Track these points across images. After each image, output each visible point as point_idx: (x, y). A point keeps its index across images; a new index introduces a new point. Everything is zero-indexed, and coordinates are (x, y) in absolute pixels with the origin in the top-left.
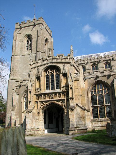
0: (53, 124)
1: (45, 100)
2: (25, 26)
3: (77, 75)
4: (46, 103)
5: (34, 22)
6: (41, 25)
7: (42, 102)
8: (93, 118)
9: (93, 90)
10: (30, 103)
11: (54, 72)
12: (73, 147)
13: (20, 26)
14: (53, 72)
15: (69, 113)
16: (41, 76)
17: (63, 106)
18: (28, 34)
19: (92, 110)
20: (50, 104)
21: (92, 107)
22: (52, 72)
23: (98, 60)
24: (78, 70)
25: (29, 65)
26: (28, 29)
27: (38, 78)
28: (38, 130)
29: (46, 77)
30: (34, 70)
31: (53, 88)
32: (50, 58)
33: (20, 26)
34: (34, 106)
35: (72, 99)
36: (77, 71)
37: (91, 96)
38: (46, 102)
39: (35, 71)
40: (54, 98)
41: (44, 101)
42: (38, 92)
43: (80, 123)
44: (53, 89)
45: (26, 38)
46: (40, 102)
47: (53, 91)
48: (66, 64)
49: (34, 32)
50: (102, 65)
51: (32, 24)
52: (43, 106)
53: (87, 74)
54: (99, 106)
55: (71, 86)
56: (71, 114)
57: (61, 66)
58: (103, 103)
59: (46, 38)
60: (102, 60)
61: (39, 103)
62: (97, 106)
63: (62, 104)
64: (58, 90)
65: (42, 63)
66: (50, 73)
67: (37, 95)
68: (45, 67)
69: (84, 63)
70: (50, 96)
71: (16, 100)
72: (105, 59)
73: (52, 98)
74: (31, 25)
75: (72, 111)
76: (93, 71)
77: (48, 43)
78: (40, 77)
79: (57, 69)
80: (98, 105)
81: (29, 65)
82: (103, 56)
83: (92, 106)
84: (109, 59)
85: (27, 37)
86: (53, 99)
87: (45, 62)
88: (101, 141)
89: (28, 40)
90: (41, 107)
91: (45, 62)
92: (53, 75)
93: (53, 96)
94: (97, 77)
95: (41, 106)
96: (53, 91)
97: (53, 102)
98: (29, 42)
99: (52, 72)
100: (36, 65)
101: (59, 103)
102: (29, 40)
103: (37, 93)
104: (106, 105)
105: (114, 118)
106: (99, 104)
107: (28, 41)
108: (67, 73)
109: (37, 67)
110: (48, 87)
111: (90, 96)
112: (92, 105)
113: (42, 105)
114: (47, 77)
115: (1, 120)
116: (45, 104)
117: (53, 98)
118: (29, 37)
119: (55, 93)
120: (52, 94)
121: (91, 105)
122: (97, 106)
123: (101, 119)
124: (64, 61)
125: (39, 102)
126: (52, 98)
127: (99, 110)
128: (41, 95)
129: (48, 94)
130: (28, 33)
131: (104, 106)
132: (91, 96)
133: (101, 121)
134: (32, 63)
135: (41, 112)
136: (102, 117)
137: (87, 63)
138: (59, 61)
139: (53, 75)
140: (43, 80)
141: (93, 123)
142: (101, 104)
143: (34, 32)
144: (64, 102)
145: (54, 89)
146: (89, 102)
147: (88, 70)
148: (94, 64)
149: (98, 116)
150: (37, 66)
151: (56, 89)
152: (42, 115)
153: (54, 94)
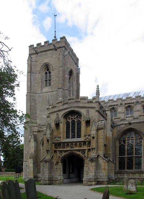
0: (74, 173)
1: (65, 149)
2: (42, 50)
4: (66, 152)
5: (54, 45)
6: (63, 49)
7: (61, 151)
8: (119, 169)
9: (126, 156)
10: (48, 152)
13: (36, 51)
16: (61, 123)
17: (84, 157)
19: (118, 161)
20: (70, 154)
21: (119, 157)
23: (134, 101)
24: (105, 116)
27: (57, 125)
28: (57, 179)
29: (67, 124)
31: (73, 137)
32: (71, 101)
33: (36, 51)
34: (52, 155)
35: (93, 150)
36: (103, 117)
37: (119, 146)
38: (66, 151)
39: (54, 117)
40: (74, 147)
41: (63, 151)
42: (57, 140)
45: (44, 69)
48: (90, 110)
50: (120, 109)
52: (62, 156)
53: (117, 119)
54: (127, 157)
57: (83, 111)
58: (132, 154)
59: (69, 70)
60: (124, 103)
61: (58, 153)
62: (125, 156)
63: (83, 154)
64: (76, 140)
65: (61, 108)
66: (70, 119)
67: (56, 144)
69: (117, 105)
72: (126, 102)
74: (50, 49)
76: (125, 117)
77: (73, 75)
78: (59, 123)
79: (79, 114)
80: (126, 156)
83: (119, 156)
84: (132, 101)
86: (73, 149)
89: (46, 72)
90: (59, 157)
92: (73, 122)
94: (130, 124)
95: (60, 156)
98: (48, 75)
100: (55, 110)
104: (128, 156)
105: (143, 171)
106: (127, 155)
107: (46, 73)
108: (90, 120)
109: (56, 111)
110: (68, 137)
111: (118, 145)
112: (119, 156)
113: (61, 155)
114: (68, 124)
116: (64, 154)
117: (73, 148)
118: (47, 67)
120: (72, 143)
121: (118, 156)
122: (125, 157)
123: (128, 170)
124: (87, 105)
125: (57, 151)
127: (127, 162)
129: (68, 143)
131: (133, 157)
132: (119, 145)
133: (127, 173)
134: (51, 107)
135: (60, 161)
137: (121, 104)
138: (81, 105)
139: (73, 122)
140: (62, 126)
141: (119, 175)
142: (129, 155)
144: (85, 153)
146: (116, 152)
147: (120, 113)
149: (125, 168)
150: (57, 110)
151: (77, 138)
152: (60, 165)
153: (82, 143)
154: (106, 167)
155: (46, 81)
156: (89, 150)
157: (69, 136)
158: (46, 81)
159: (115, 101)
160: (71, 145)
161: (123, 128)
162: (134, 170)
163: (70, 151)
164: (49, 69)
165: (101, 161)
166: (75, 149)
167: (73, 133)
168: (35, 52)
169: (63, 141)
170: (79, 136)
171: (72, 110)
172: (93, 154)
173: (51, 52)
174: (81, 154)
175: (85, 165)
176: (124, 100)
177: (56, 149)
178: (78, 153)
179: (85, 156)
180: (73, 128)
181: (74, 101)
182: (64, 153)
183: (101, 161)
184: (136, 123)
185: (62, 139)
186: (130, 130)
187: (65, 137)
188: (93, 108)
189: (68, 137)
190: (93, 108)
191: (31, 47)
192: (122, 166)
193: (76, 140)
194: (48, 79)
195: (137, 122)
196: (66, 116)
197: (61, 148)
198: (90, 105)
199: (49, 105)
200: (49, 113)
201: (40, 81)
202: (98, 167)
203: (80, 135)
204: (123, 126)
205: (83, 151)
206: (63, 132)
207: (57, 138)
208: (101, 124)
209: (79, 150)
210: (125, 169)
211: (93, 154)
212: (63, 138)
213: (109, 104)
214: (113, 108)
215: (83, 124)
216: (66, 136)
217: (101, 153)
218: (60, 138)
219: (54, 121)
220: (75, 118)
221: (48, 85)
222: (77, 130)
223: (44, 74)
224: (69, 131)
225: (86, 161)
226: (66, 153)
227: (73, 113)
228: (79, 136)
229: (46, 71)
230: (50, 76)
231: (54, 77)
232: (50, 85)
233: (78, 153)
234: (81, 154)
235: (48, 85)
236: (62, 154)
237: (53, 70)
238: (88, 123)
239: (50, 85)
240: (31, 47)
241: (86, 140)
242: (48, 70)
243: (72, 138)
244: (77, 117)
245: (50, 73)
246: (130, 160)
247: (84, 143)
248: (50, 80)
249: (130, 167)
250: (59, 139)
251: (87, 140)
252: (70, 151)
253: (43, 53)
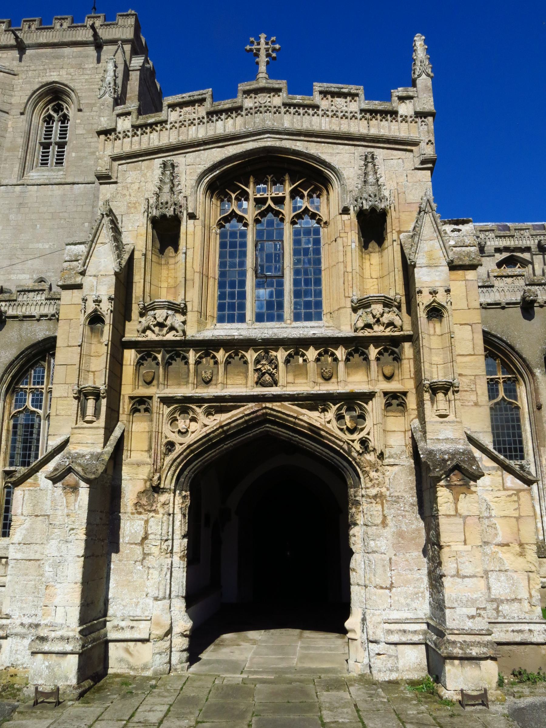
2: (43, 40)
3: (459, 230)
11: (283, 198)
12: (298, 683)
14: (273, 199)
15: (440, 500)
16: (192, 216)
17: (357, 446)
18: (47, 84)
22: (270, 202)
25: (99, 133)
26: (57, 57)
30: (135, 169)
41: (200, 401)
42: (161, 325)
43: (496, 592)
44: (271, 319)
46: (166, 401)
47: (275, 331)
48: (380, 154)
49: (87, 77)
51: (79, 39)
52: (190, 439)
55: (441, 298)
56: (457, 514)
63: (351, 431)
68: (208, 165)
70: (251, 367)
71: (366, 492)
73: (267, 377)
74: (74, 39)
75: (463, 489)
78: (176, 221)
81: (99, 133)
85: (49, 98)
89: (50, 117)
90: (171, 445)
93: (276, 367)
96: (275, 331)
97: (276, 406)
98: (56, 126)
99: (266, 199)
102: (55, 115)
103: (151, 336)
107: (49, 119)
126: (267, 377)
130: (53, 77)
143: (87, 77)
145: (280, 318)
155: (46, 146)
157: (242, 307)
158: (46, 146)
160: (257, 361)
163: (251, 407)
164: (65, 105)
166: (291, 390)
167: (264, 293)
168: (13, 42)
169: (200, 336)
171: (265, 148)
174: (334, 427)
177: (143, 391)
179: (364, 442)
181: (277, 101)
182: (202, 418)
185: (191, 317)
187: (212, 308)
194: (55, 137)
195: (489, 301)
197: (183, 380)
199: (119, 115)
200: (115, 159)
203: (319, 305)
206: (204, 276)
207: (161, 314)
212: (202, 314)
216: (221, 307)
218: (183, 311)
219: (142, 208)
220: (279, 201)
221: (52, 159)
222: (297, 272)
223: (38, 120)
224: (243, 274)
229: (52, 113)
230: (64, 132)
231: (80, 131)
232: (59, 162)
234: (334, 427)
235: (52, 159)
236: (193, 426)
237: (80, 110)
241: (367, 333)
243: (259, 318)
244: (294, 194)
245: (65, 119)
248: (62, 145)
250: (177, 320)
251: (378, 331)
252: (251, 407)
253: (48, 50)
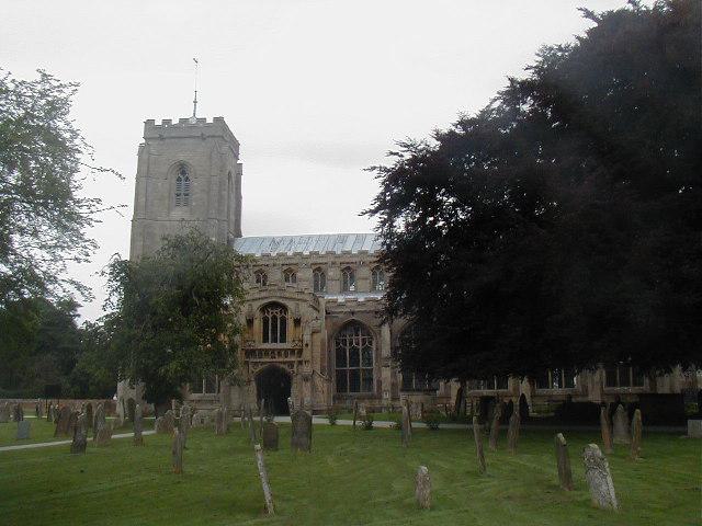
1: (262, 360)
2: (173, 135)
9: (348, 367)
23: (357, 259)
27: (250, 322)
31: (275, 340)
38: (263, 363)
57: (290, 305)
60: (338, 261)
64: (279, 346)
79: (284, 308)
80: (348, 367)
82: (339, 253)
87: (263, 294)
88: (528, 400)
91: (263, 294)
92: (274, 318)
98: (183, 182)
101: (286, 367)
107: (179, 179)
110: (265, 340)
115: (12, 297)
116: (260, 367)
119: (279, 351)
120: (273, 351)
128: (253, 351)
129: (267, 351)
136: (337, 358)
139: (274, 318)
140: (258, 324)
148: (319, 269)
152: (253, 386)
154: (325, 389)
156: (300, 363)
159: (322, 257)
161: (342, 319)
162: (362, 393)
165: (318, 381)
170: (283, 340)
172: (307, 369)
173: (192, 141)
175: (294, 385)
176: (339, 257)
178: (282, 366)
180: (274, 327)
183: (318, 381)
184: (362, 312)
186: (353, 323)
188: (306, 301)
189: (265, 340)
190: (306, 301)
191: (149, 123)
192: (341, 387)
193: (279, 346)
196: (264, 309)
198: (300, 297)
201: (166, 195)
202: (314, 388)
204: (341, 316)
205: (291, 364)
208: (316, 324)
209: (284, 363)
210: (346, 391)
211: (307, 369)
213: (311, 261)
214: (319, 269)
215: (290, 324)
217: (318, 368)
223: (174, 181)
225: (296, 381)
226: (264, 366)
227: (274, 305)
228: (283, 340)
233: (282, 366)
238: (297, 322)
239: (186, 205)
240: (149, 123)
242: (183, 173)
246: (355, 374)
247: (293, 351)
249: (355, 388)
